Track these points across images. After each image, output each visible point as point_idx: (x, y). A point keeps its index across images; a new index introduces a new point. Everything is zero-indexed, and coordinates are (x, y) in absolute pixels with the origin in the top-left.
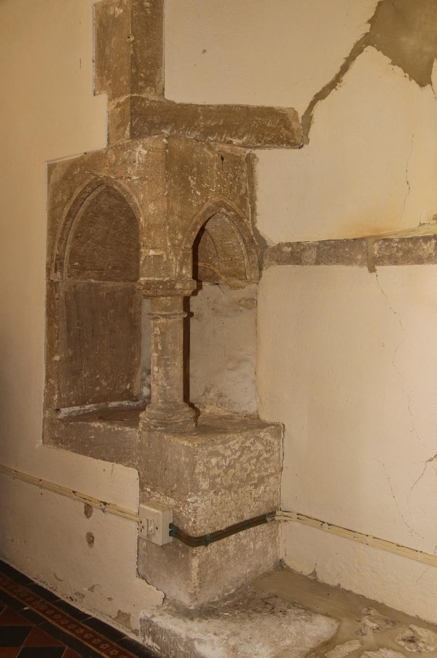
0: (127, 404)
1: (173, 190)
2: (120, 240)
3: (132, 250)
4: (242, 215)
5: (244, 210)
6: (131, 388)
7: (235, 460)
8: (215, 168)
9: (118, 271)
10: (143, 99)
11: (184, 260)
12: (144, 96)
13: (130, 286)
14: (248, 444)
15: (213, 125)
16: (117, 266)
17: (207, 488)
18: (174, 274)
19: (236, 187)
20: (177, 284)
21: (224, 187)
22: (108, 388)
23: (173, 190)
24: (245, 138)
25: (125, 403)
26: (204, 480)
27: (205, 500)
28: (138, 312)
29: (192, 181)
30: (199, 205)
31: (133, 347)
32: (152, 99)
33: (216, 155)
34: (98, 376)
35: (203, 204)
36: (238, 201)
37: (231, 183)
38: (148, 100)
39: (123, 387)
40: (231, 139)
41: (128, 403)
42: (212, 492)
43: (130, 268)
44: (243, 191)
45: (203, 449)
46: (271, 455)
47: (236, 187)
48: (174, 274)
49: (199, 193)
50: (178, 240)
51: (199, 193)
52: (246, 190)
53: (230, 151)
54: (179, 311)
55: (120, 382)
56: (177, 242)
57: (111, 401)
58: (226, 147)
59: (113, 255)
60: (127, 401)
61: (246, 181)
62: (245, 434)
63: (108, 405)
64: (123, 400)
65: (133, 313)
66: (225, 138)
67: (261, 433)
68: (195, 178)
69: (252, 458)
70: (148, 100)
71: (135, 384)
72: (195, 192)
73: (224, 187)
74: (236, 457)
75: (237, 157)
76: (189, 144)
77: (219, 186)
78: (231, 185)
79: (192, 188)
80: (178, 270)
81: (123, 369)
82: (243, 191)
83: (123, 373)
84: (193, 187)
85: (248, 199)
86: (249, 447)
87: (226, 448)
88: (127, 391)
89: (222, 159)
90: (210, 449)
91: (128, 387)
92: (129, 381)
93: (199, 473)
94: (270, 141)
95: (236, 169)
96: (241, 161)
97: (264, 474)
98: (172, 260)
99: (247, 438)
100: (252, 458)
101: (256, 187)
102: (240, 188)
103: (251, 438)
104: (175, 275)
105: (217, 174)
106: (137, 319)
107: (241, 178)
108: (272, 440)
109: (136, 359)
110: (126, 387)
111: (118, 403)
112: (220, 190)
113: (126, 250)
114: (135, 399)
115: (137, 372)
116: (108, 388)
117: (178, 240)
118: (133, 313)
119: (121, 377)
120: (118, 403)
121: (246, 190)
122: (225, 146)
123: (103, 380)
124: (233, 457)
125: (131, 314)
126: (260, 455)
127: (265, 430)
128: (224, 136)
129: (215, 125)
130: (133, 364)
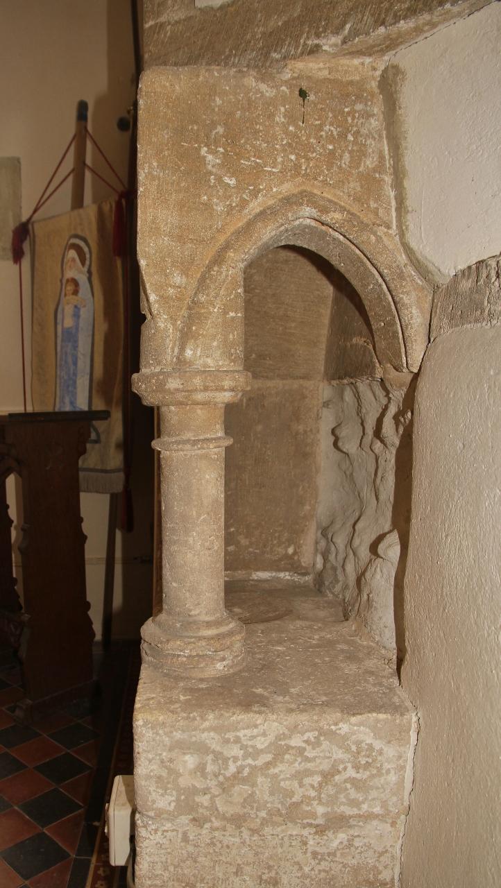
0: (289, 578)
1: (156, 182)
2: (264, 310)
3: (293, 325)
4: (367, 218)
5: (373, 205)
6: (295, 553)
7: (253, 768)
8: (280, 119)
9: (271, 362)
10: (162, 25)
11: (190, 328)
12: (162, 19)
13: (295, 386)
14: (296, 741)
15: (280, 24)
16: (267, 352)
17: (172, 808)
18: (169, 358)
19: (347, 155)
20: (170, 380)
21: (308, 159)
22: (251, 550)
23: (156, 182)
24: (348, 26)
25: (285, 576)
26: (161, 791)
27: (165, 828)
28: (311, 430)
29: (210, 157)
30: (231, 208)
31: (301, 488)
32: (176, 18)
33: (284, 88)
34: (232, 530)
35: (243, 204)
36: (354, 186)
37: (331, 147)
38: (169, 23)
39: (281, 550)
40: (316, 42)
41: (291, 576)
42: (184, 819)
43: (293, 356)
44: (370, 163)
45: (157, 734)
46: (372, 776)
47: (347, 155)
48: (169, 358)
49: (232, 182)
50: (174, 287)
51: (232, 182)
52: (382, 157)
53: (326, 73)
54: (194, 436)
55: (275, 542)
56: (171, 291)
57: (257, 570)
58: (316, 66)
59: (257, 335)
60: (287, 573)
61: (380, 136)
62: (292, 719)
63: (251, 575)
64: (280, 570)
65: (301, 431)
66: (305, 44)
67: (341, 725)
68: (221, 150)
69: (308, 773)
70: (169, 23)
71: (304, 547)
72: (219, 179)
73: (308, 159)
74: (260, 762)
75: (351, 83)
76: (201, 79)
77: (293, 157)
78: (332, 153)
79: (211, 173)
80: (176, 350)
81: (281, 521)
82: (370, 163)
83: (280, 529)
84: (214, 170)
85: (386, 179)
86: (301, 751)
87: (227, 741)
88: (287, 556)
89: (303, 94)
90: (178, 735)
91: (291, 551)
92: (290, 542)
93: (148, 777)
94: (408, 9)
95: (348, 113)
96: (365, 90)
97: (348, 811)
98: (166, 329)
99: (294, 729)
100: (308, 773)
101: (404, 145)
102: (360, 153)
103: (307, 731)
104: (172, 361)
105: (286, 132)
106: (309, 441)
107: (364, 131)
108: (378, 745)
109: (307, 507)
110: (286, 551)
111: (270, 575)
112: (297, 167)
113: (282, 325)
114: (303, 571)
115: (308, 529)
116: (251, 550)
117: (174, 287)
118: (301, 431)
119: (277, 535)
120: (270, 575)
121: (382, 157)
122: (311, 65)
123: (242, 536)
124: (250, 761)
125: (297, 433)
126: (334, 771)
127: (353, 719)
128: (302, 41)
129: (285, 23)
130: (302, 515)
